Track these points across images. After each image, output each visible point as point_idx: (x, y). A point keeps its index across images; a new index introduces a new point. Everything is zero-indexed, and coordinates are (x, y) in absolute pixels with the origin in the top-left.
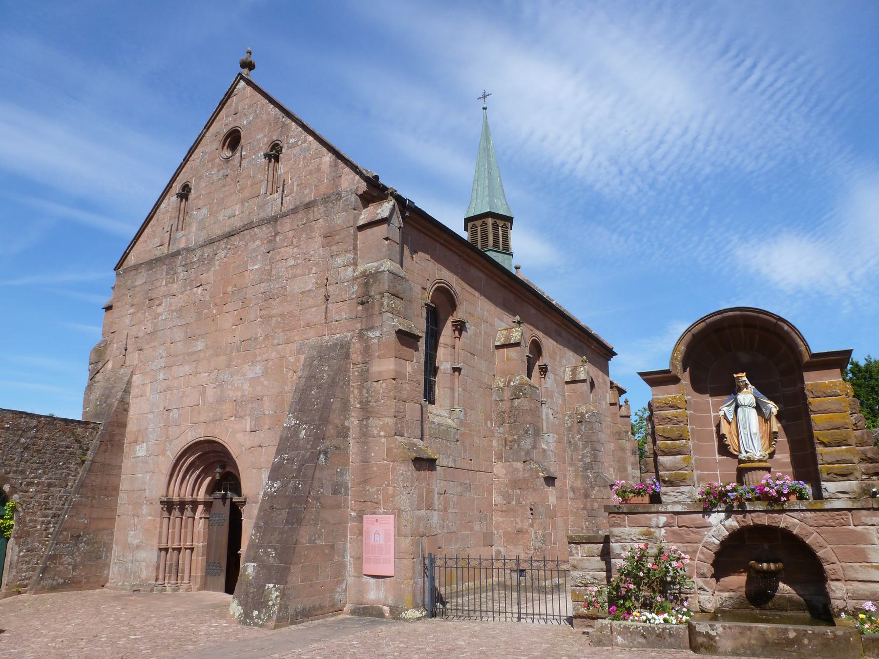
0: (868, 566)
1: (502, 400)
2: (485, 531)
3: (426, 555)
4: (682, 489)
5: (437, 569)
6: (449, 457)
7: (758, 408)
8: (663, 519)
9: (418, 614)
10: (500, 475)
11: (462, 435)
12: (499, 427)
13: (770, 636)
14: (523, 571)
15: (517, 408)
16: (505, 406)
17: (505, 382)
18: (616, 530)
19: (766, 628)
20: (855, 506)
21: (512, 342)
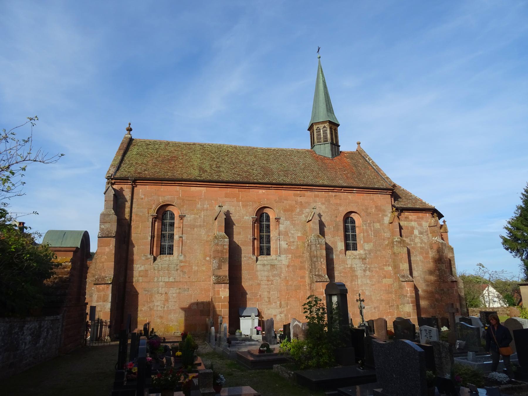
6: (169, 277)
11: (181, 267)
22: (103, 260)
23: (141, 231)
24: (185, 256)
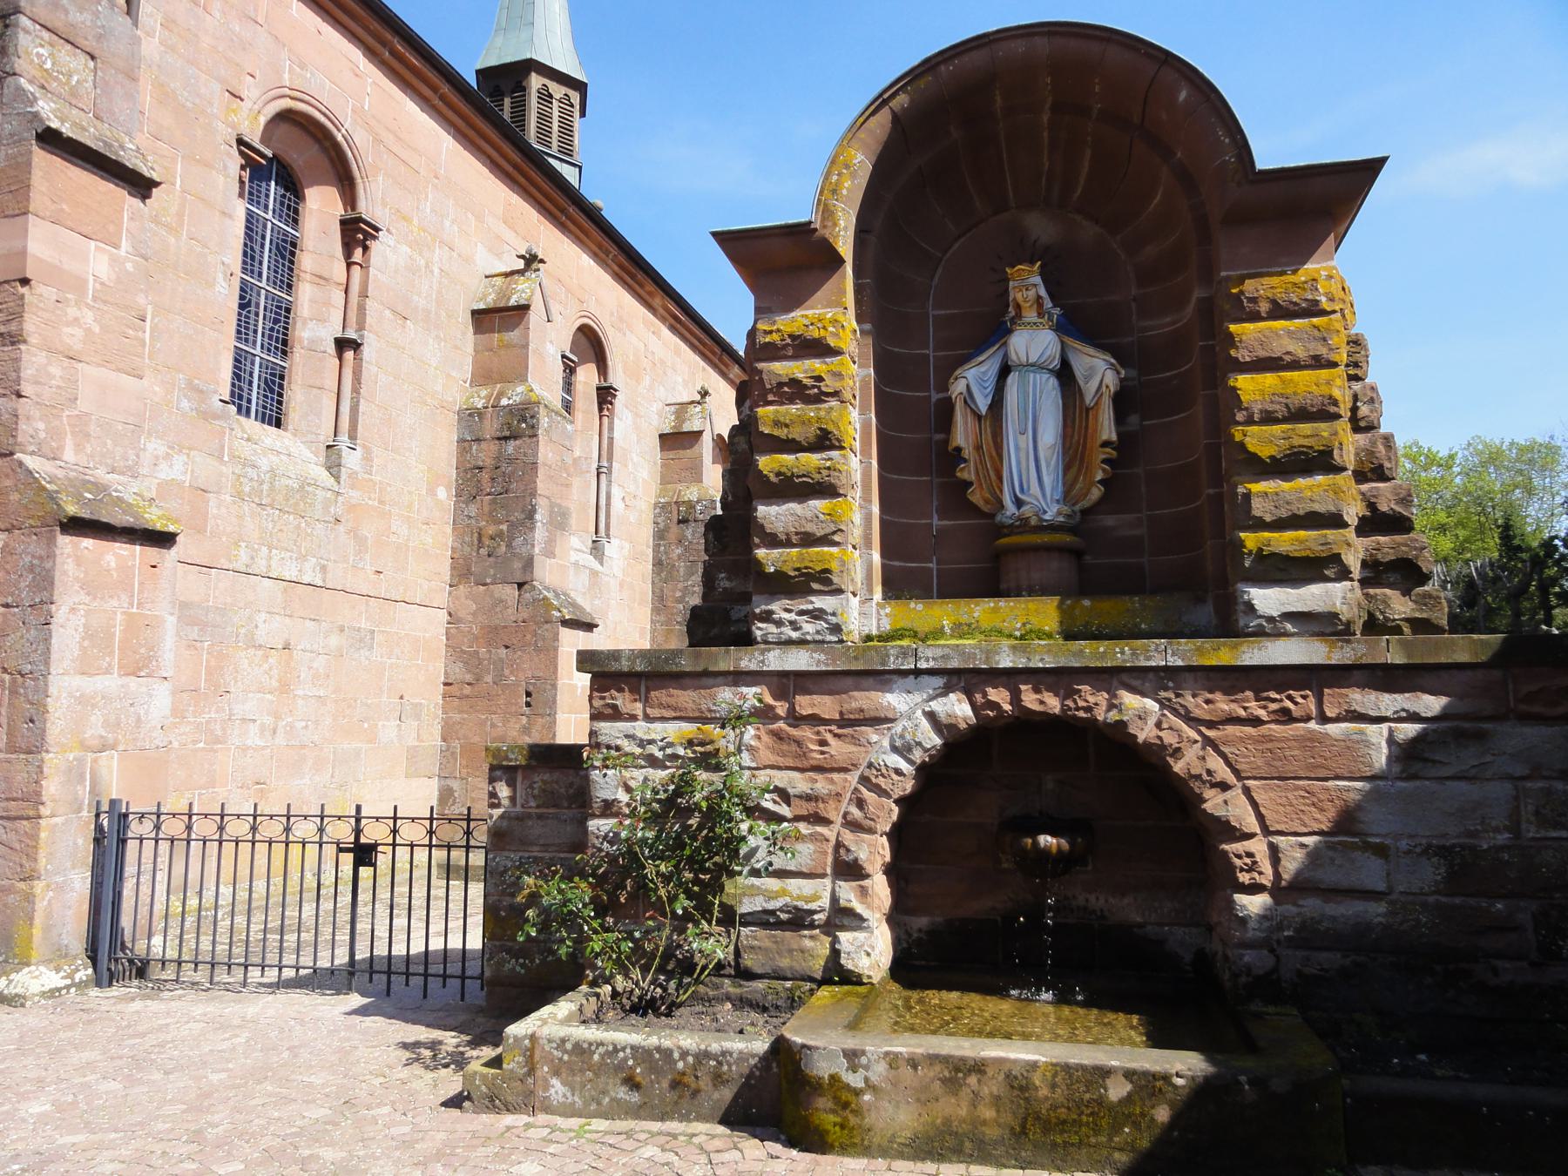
0: (1354, 847)
1: (478, 440)
2: (412, 742)
3: (105, 807)
4: (819, 602)
5: (132, 846)
7: (1065, 374)
8: (752, 695)
9: (53, 979)
10: (462, 614)
11: (352, 508)
12: (467, 504)
13: (1044, 1092)
14: (373, 848)
15: (511, 460)
16: (485, 454)
17: (488, 398)
18: (611, 731)
19: (1034, 1066)
20: (1341, 655)
21: (512, 302)
22: (72, 337)
23: (180, 215)
24: (368, 458)
